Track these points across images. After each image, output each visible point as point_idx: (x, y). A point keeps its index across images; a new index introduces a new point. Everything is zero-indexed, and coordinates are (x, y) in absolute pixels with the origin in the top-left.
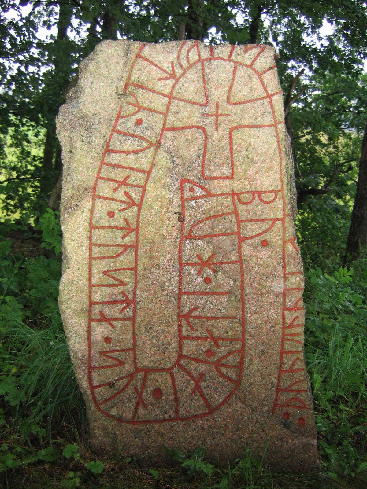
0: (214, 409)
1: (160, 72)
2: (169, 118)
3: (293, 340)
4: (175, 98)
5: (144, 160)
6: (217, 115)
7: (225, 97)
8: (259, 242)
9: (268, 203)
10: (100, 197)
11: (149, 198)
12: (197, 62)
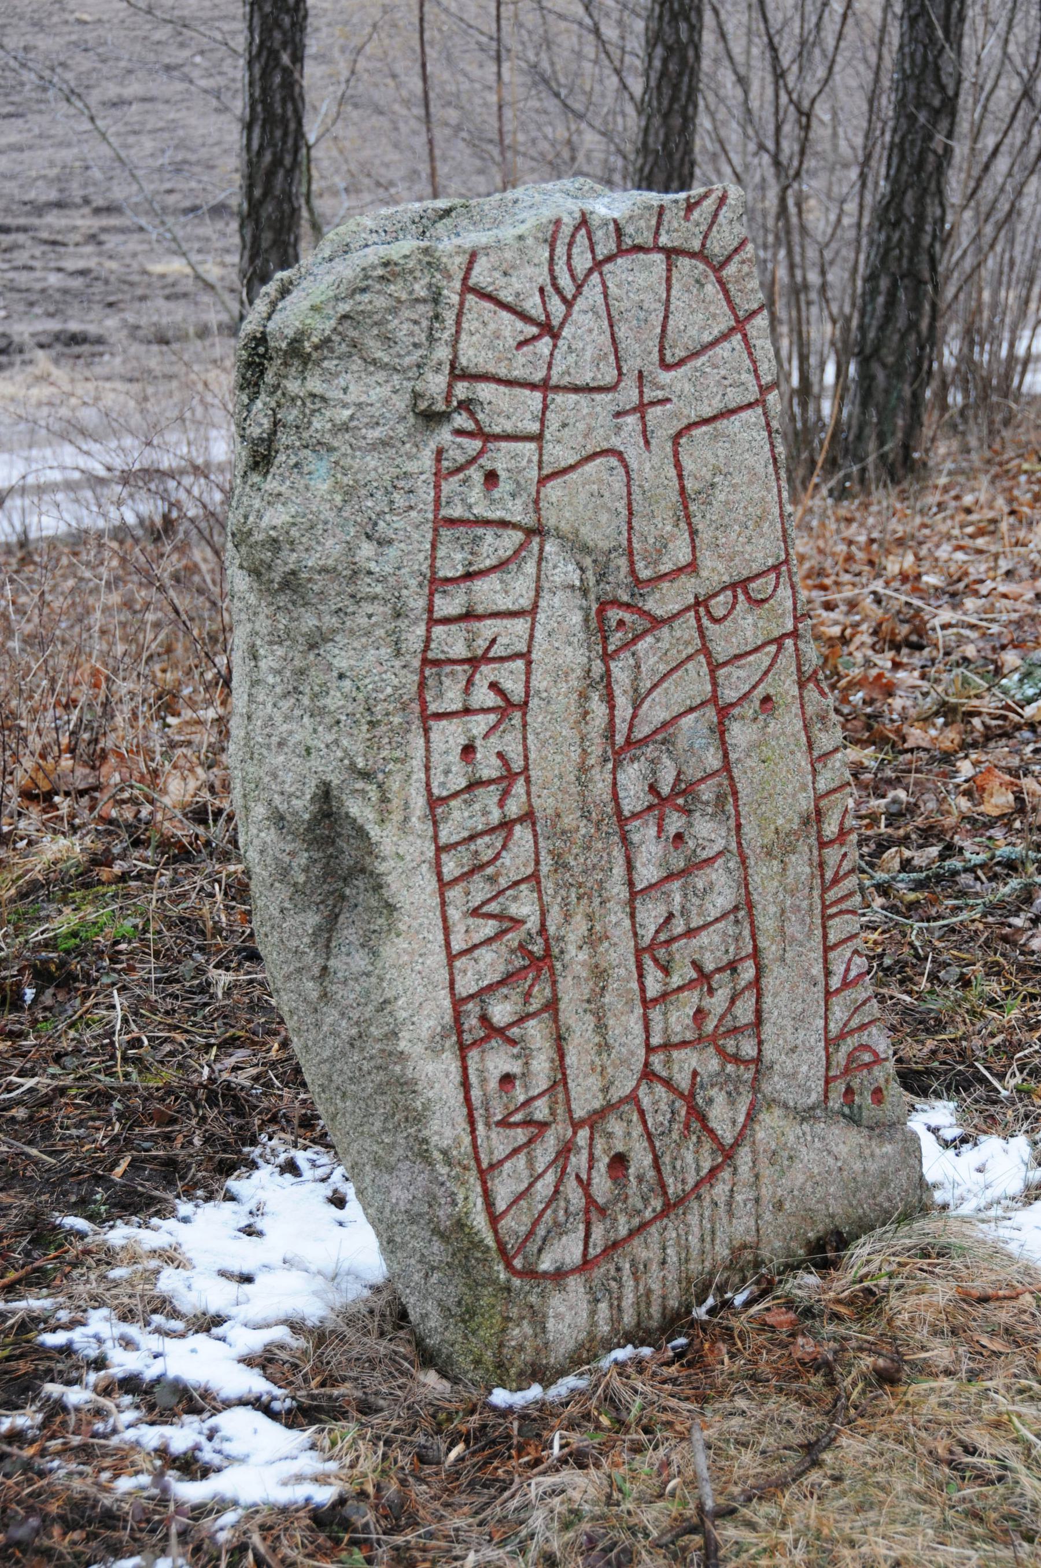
0: (732, 1146)
1: (520, 325)
2: (548, 447)
3: (841, 912)
4: (557, 388)
5: (518, 590)
6: (641, 408)
7: (655, 356)
8: (186, 13)
9: (763, 601)
10: (439, 716)
11: (540, 681)
12: (590, 271)
